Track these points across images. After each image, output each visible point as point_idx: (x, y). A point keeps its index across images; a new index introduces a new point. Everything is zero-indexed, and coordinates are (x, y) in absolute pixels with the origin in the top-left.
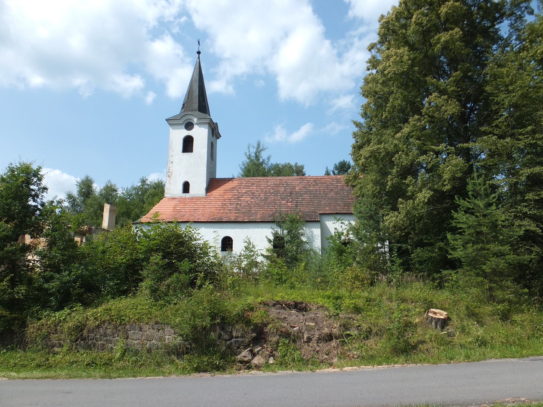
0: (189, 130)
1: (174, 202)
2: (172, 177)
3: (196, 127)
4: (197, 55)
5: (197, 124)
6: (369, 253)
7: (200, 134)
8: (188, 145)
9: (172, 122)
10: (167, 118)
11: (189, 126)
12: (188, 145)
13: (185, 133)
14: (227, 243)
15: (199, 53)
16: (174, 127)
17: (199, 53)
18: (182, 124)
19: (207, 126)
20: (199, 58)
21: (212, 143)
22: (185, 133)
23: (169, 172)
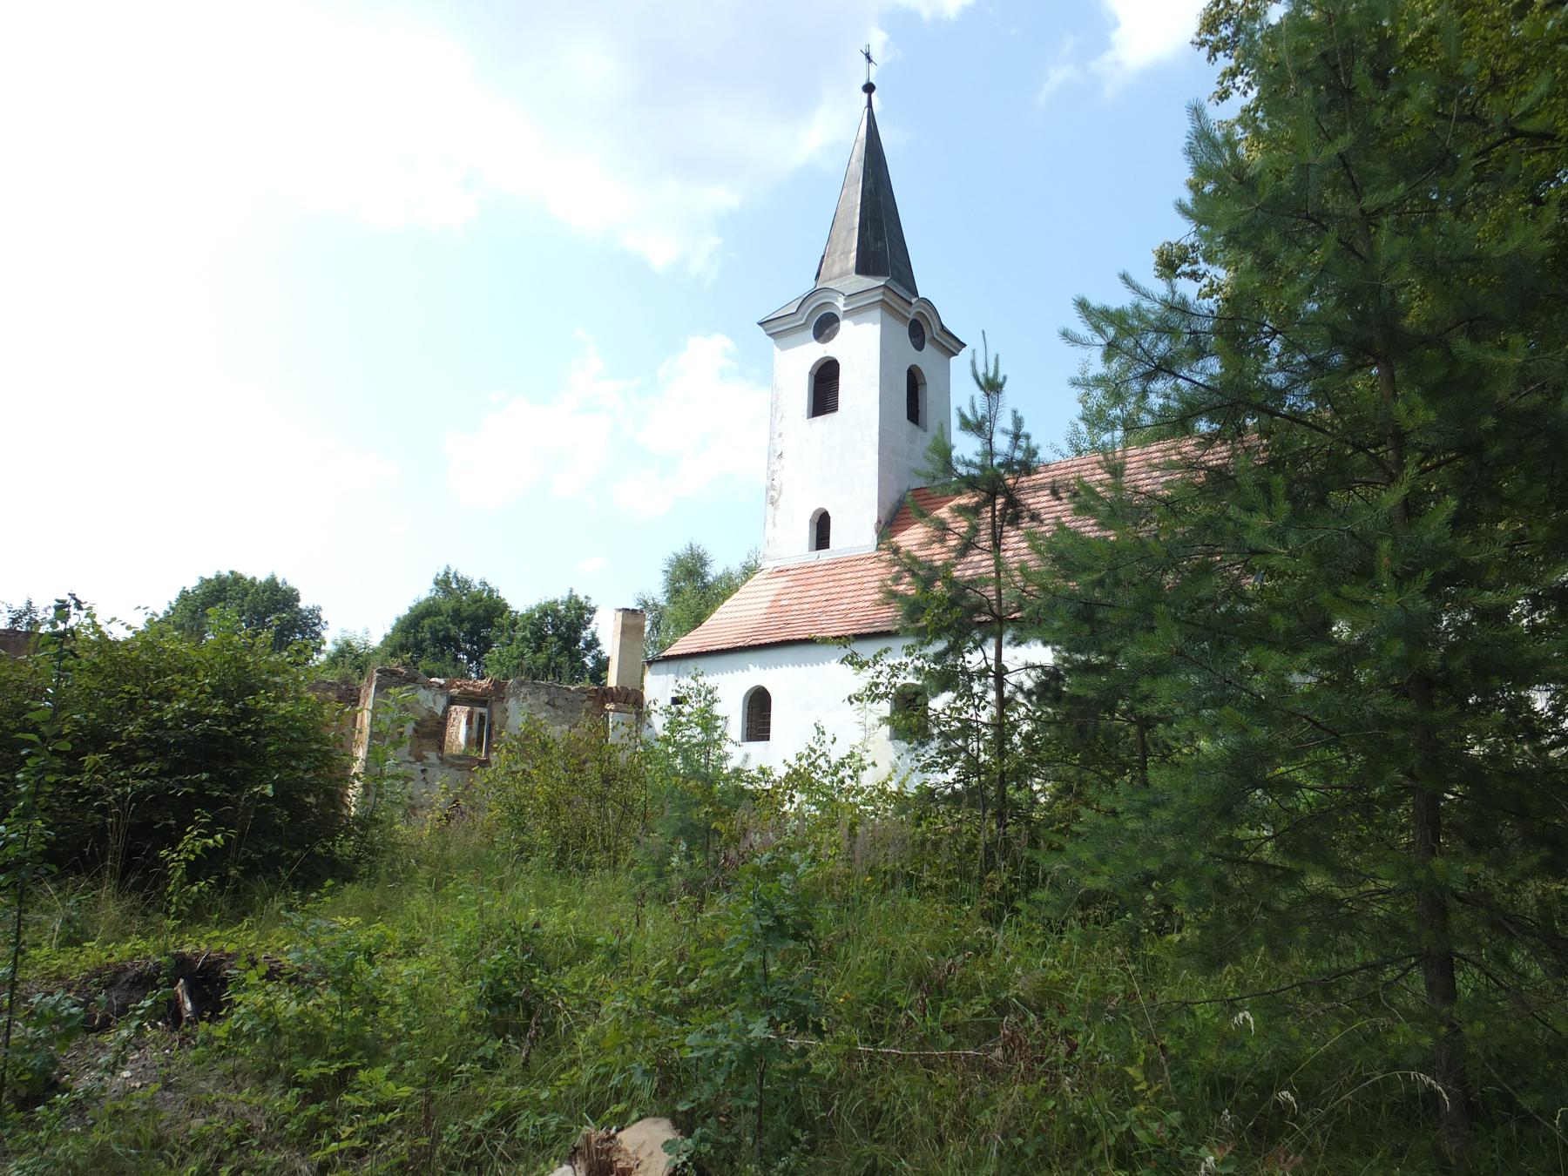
0: (825, 342)
1: (781, 583)
2: (781, 502)
3: (846, 326)
4: (865, 96)
5: (847, 314)
6: (1227, 808)
7: (860, 347)
8: (824, 388)
9: (777, 328)
10: (760, 319)
11: (825, 326)
12: (824, 388)
13: (812, 352)
14: (759, 706)
15: (869, 88)
16: (784, 340)
17: (869, 88)
18: (804, 326)
19: (877, 313)
20: (870, 105)
21: (914, 381)
22: (812, 352)
23: (773, 487)
